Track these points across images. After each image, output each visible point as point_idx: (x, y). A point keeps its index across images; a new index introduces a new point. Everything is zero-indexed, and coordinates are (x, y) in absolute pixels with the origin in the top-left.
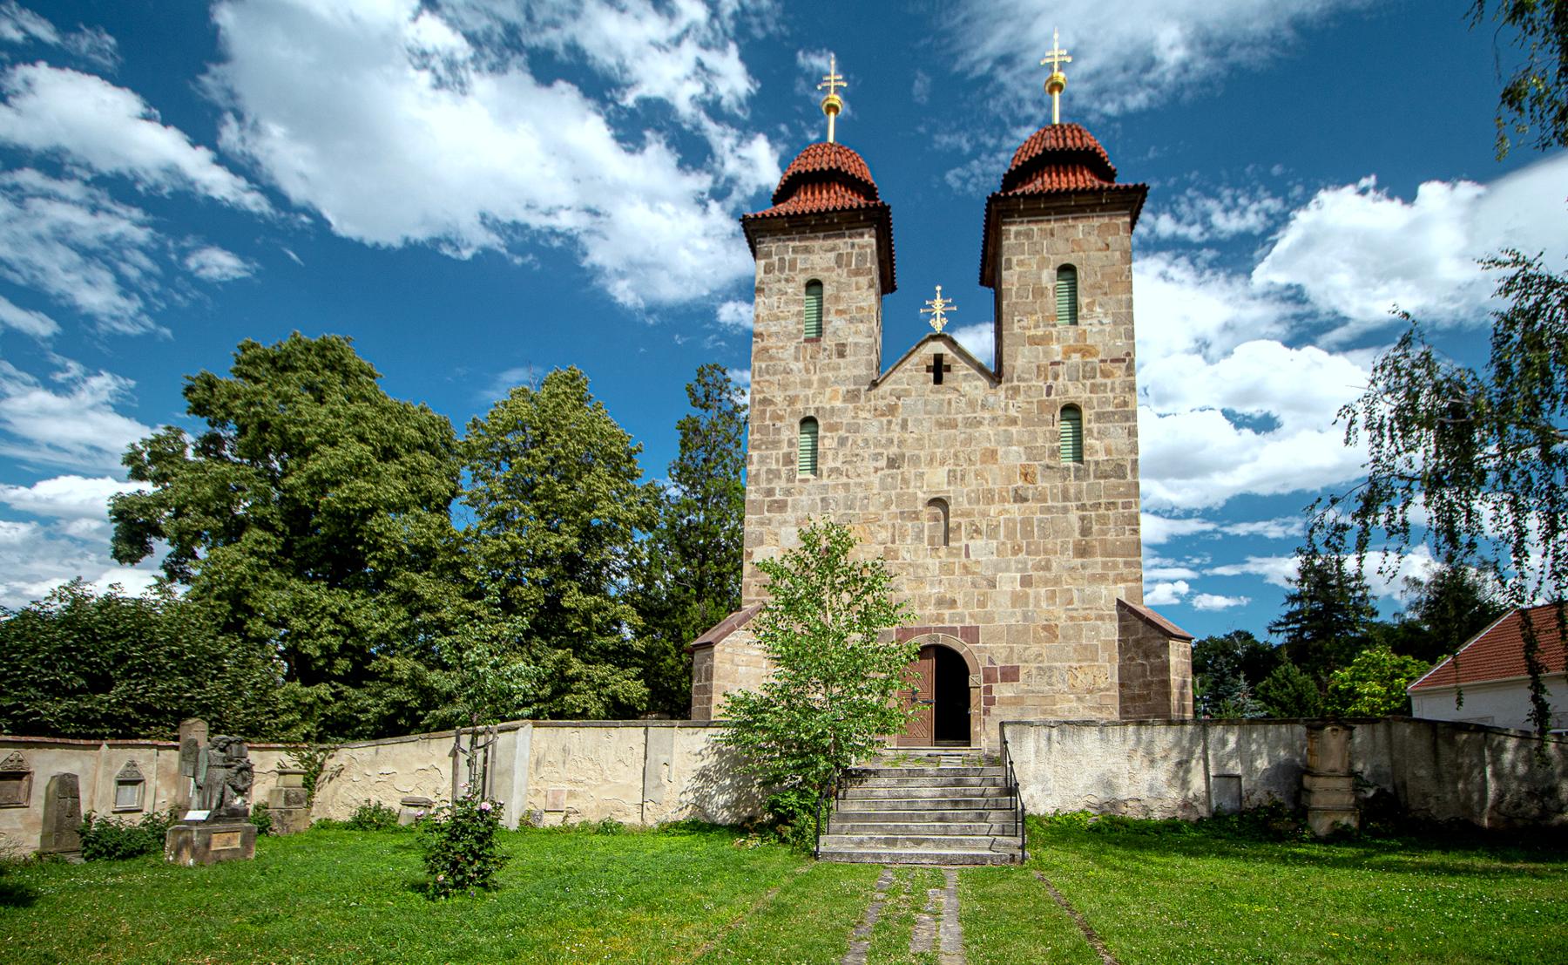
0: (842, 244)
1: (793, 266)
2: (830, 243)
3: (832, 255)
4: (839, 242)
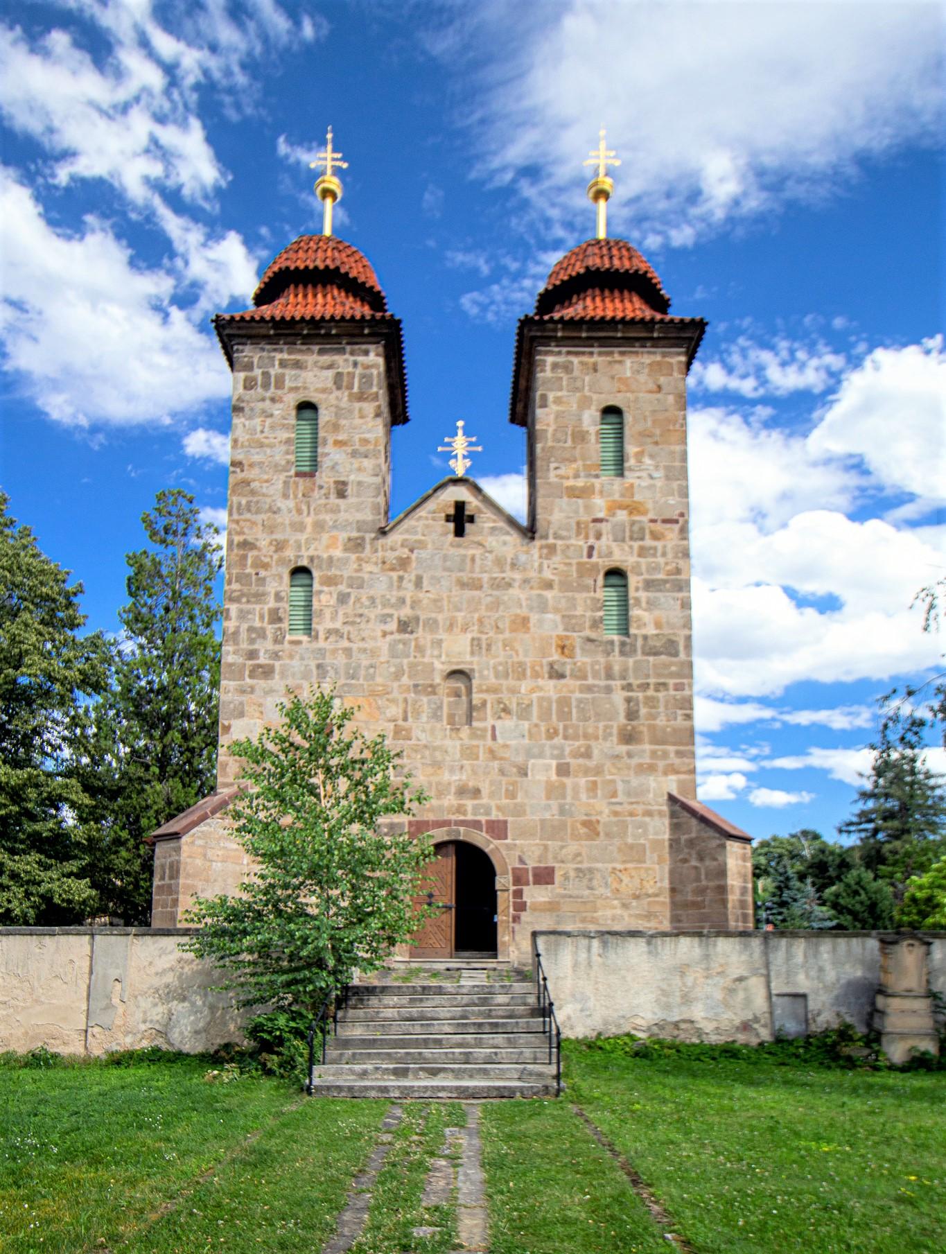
0: (343, 361)
1: (280, 383)
2: (326, 359)
3: (330, 374)
4: (339, 359)
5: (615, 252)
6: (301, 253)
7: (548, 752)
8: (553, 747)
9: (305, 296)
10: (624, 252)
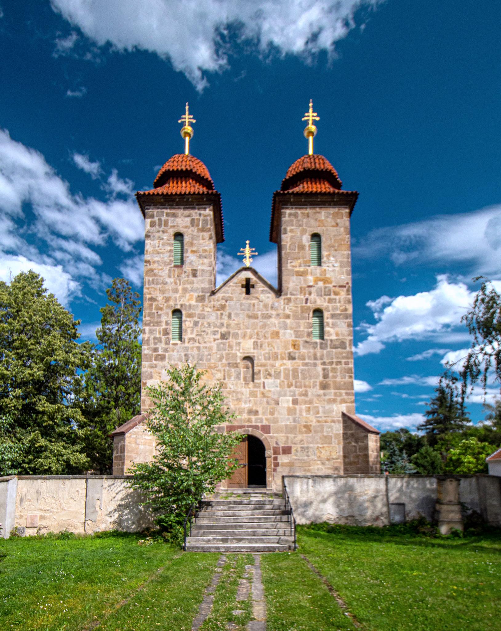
0: (195, 213)
1: (166, 224)
2: (187, 212)
3: (189, 219)
4: (193, 212)
5: (317, 161)
6: (175, 163)
7: (288, 394)
8: (291, 391)
9: (177, 183)
10: (321, 161)
